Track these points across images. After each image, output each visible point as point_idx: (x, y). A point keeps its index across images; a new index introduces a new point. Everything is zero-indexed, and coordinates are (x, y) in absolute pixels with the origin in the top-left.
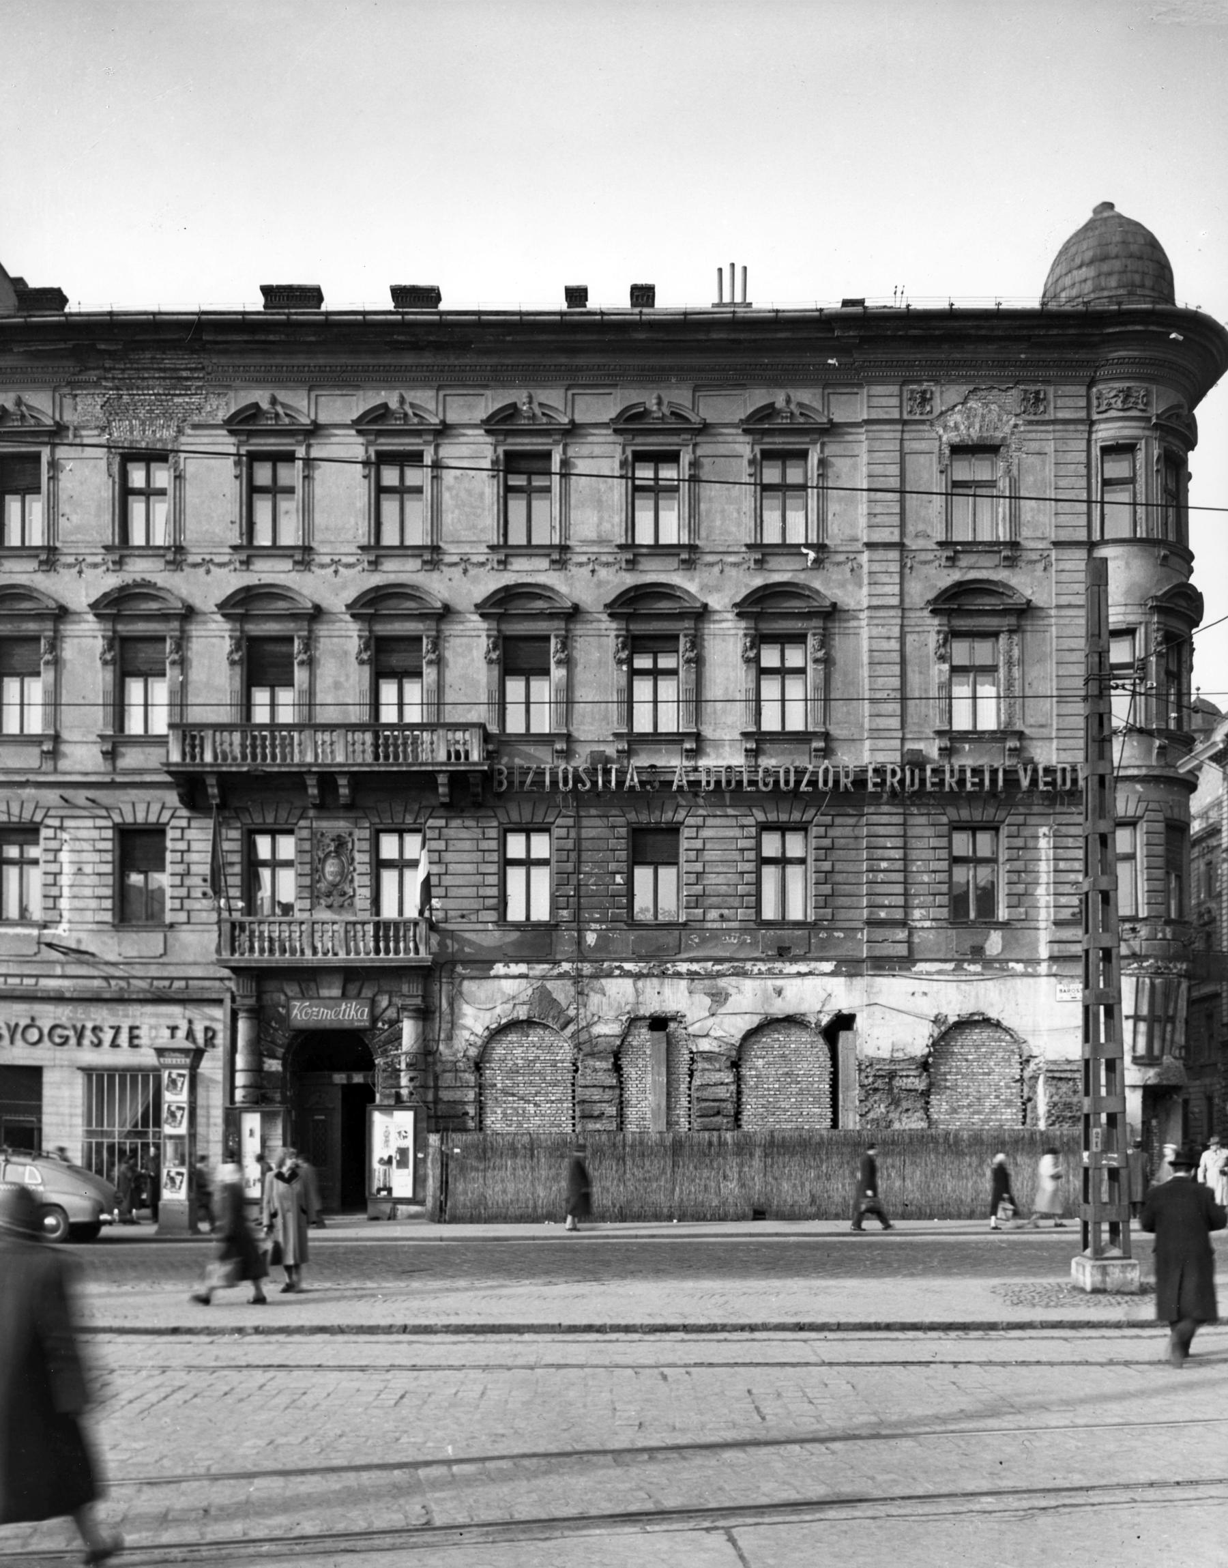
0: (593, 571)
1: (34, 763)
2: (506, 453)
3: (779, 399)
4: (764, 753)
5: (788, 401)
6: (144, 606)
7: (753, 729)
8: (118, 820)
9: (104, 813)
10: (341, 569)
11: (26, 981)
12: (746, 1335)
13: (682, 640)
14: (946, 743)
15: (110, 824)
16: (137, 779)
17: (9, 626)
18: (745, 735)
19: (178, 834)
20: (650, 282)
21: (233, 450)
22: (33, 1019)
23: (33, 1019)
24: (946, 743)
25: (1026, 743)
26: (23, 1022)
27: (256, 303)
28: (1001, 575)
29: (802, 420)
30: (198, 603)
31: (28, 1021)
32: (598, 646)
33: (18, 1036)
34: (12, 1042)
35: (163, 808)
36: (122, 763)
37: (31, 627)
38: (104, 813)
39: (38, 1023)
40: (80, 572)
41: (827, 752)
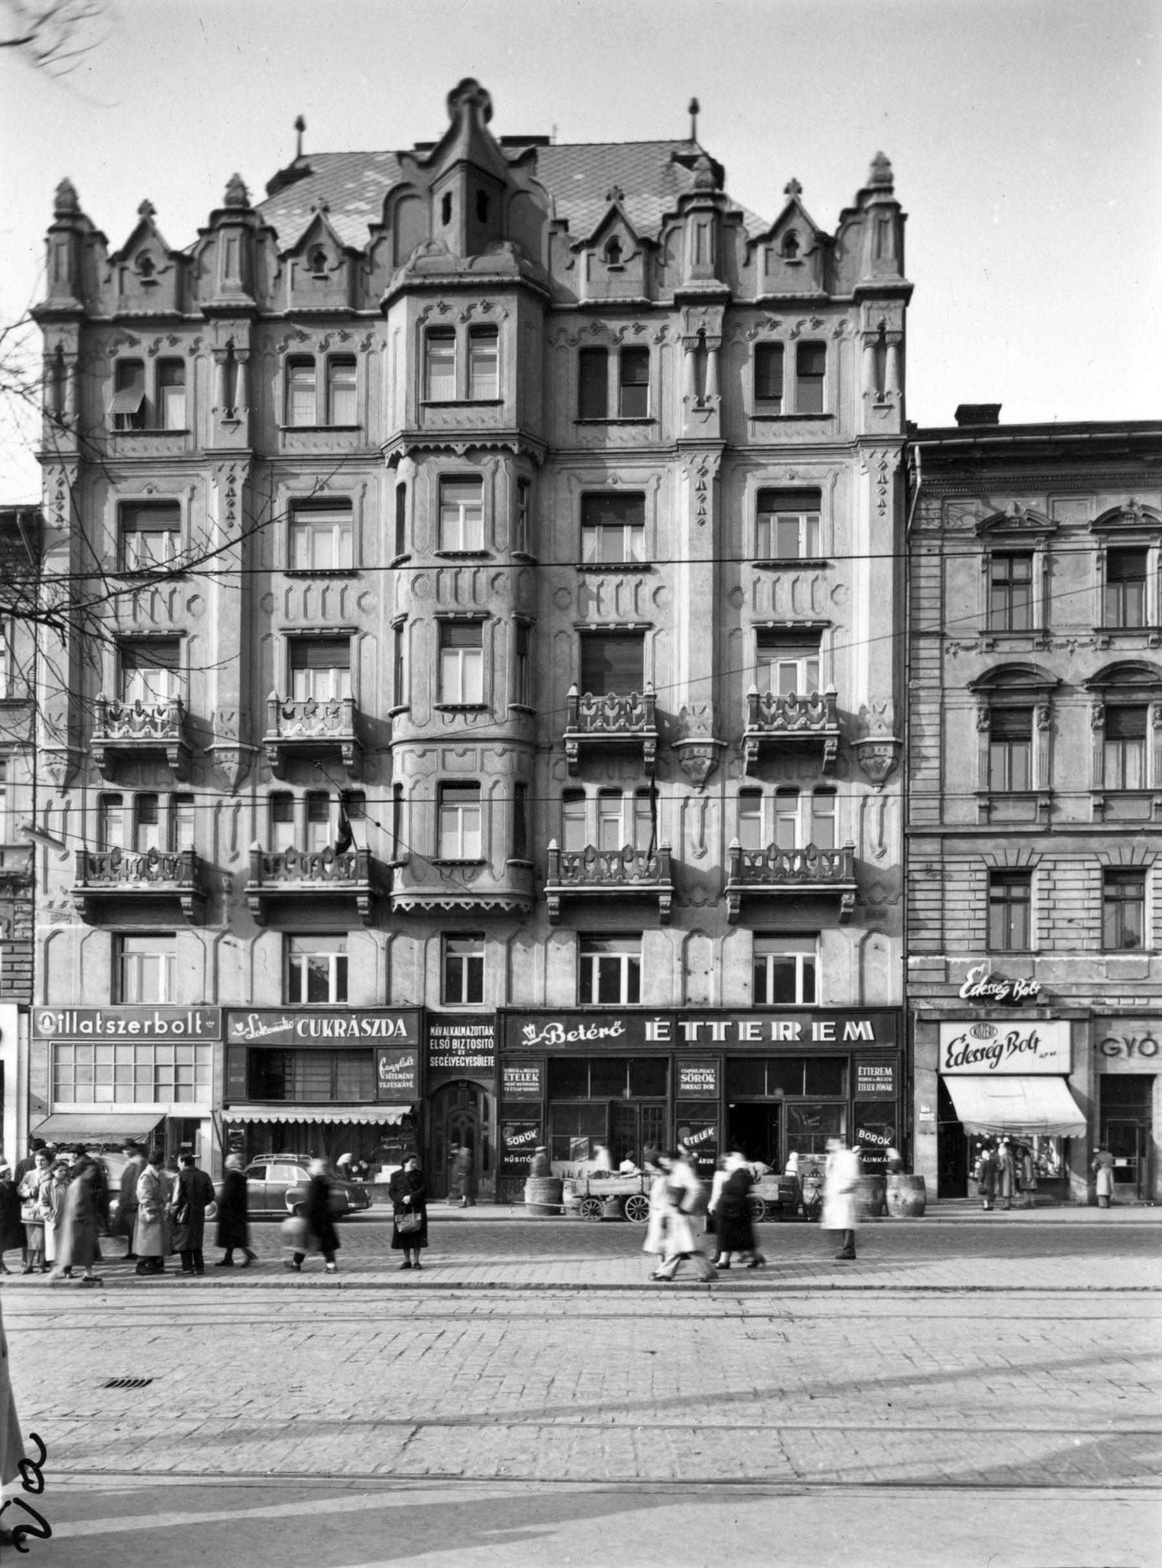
0: (1072, 651)
1: (1029, 815)
2: (1109, 549)
3: (1007, 505)
4: (996, 808)
5: (1017, 509)
6: (1018, 681)
7: (986, 789)
8: (991, 862)
9: (1093, 857)
10: (1078, 650)
11: (1137, 1001)
12: (938, 1294)
13: (1036, 712)
14: (1099, 800)
15: (984, 867)
16: (1012, 829)
17: (1120, 697)
18: (979, 794)
19: (1043, 875)
20: (997, 402)
21: (1096, 546)
22: (1149, 1034)
23: (1149, 1034)
24: (1099, 800)
25: (1055, 801)
26: (1140, 1037)
27: (953, 423)
28: (1032, 658)
29: (1144, 520)
30: (1067, 679)
31: (1144, 1036)
32: (1080, 716)
33: (1136, 1049)
34: (1130, 1054)
35: (1032, 853)
36: (997, 815)
37: (1141, 696)
38: (978, 858)
39: (1154, 1037)
40: (1072, 651)
41: (1049, 809)
